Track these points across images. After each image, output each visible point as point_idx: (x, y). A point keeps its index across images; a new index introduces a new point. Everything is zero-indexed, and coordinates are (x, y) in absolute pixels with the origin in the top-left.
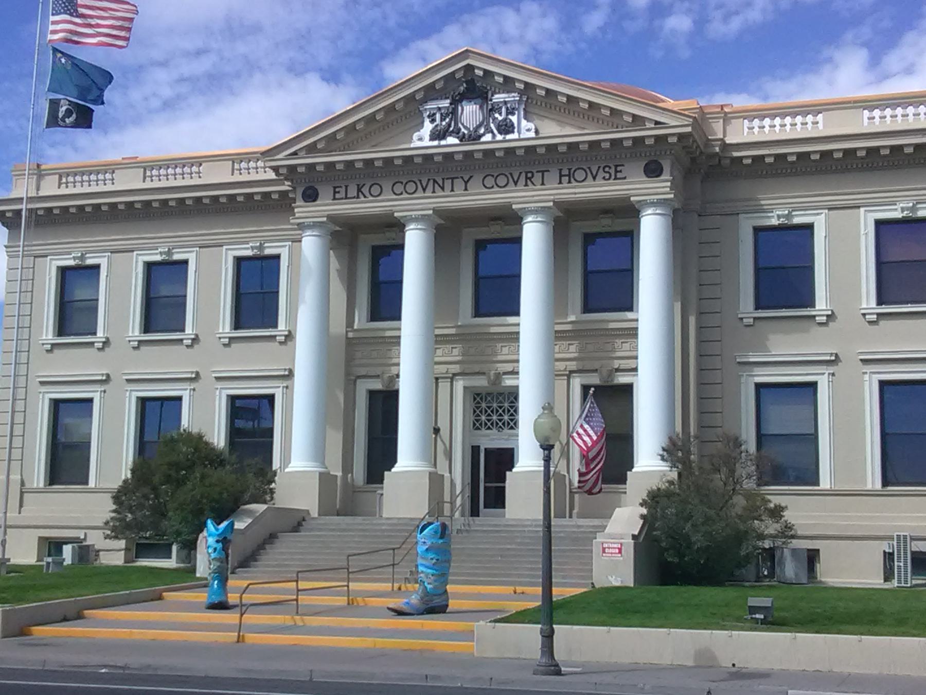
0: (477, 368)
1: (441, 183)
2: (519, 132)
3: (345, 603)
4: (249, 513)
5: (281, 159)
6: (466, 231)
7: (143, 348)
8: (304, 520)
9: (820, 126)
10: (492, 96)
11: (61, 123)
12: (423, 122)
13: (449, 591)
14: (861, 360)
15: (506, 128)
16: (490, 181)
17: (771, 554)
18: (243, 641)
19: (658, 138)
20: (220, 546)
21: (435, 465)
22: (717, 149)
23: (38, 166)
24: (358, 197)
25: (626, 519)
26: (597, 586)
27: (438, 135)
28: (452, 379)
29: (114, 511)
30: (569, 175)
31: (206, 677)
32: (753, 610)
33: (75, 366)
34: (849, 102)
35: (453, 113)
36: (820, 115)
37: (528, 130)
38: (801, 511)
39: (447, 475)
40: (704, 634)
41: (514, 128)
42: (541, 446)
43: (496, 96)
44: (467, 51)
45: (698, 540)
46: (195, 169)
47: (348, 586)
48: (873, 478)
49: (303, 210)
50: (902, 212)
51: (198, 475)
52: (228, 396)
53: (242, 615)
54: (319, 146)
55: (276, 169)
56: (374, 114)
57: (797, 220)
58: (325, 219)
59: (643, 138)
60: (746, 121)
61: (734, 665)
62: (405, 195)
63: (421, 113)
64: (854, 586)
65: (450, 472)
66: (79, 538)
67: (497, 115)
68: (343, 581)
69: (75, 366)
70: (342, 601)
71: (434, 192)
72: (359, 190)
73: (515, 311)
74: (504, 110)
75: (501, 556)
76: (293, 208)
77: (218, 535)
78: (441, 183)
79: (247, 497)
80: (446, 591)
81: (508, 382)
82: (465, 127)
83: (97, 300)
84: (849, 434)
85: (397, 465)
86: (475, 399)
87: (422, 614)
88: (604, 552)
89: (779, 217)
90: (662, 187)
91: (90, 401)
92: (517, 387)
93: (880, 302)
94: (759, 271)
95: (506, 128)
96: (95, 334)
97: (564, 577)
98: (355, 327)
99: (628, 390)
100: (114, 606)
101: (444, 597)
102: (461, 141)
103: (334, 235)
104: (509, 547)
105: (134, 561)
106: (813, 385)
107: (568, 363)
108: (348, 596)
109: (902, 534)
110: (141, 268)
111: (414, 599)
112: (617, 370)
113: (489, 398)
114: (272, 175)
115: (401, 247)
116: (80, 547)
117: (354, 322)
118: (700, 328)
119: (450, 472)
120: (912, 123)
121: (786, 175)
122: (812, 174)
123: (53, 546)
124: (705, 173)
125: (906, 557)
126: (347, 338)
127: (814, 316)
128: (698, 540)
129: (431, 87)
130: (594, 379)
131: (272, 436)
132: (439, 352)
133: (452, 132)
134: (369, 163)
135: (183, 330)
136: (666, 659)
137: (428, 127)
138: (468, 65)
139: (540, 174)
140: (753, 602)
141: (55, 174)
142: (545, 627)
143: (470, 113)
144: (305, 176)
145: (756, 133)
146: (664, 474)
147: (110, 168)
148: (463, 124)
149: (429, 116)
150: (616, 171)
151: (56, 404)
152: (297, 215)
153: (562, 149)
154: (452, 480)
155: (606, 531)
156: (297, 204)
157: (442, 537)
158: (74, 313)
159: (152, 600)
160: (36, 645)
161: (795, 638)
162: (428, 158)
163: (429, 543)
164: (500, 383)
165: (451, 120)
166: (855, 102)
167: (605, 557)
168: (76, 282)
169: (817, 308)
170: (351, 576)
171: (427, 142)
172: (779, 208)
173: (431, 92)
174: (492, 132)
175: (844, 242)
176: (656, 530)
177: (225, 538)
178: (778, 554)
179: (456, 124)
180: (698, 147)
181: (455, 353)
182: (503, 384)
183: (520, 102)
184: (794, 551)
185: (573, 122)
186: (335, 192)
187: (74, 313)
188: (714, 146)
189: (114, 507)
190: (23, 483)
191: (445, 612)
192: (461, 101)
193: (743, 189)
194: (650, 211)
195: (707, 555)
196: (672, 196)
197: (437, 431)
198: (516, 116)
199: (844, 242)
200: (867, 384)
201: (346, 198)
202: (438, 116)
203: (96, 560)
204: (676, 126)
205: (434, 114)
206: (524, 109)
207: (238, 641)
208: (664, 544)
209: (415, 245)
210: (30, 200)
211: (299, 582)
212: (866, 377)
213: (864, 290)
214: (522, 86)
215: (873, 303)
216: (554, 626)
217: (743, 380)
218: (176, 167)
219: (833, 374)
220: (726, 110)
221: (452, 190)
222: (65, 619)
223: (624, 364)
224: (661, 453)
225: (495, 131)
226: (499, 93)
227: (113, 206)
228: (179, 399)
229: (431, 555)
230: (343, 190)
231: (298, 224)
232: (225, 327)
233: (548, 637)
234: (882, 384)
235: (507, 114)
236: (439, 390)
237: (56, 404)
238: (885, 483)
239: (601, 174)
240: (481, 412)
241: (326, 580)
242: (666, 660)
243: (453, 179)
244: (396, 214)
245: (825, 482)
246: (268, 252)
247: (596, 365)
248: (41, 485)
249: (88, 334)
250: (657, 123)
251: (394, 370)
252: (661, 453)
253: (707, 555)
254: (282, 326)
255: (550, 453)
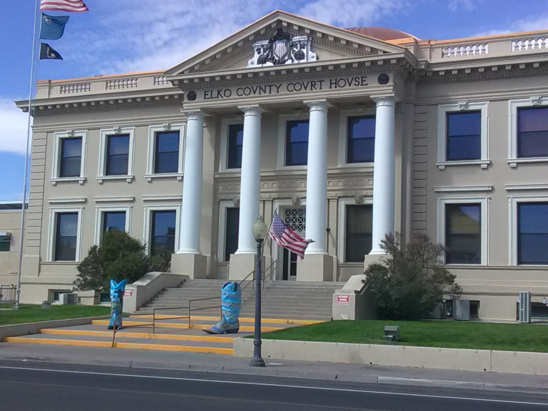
0: (286, 195)
1: (264, 88)
2: (307, 59)
3: (188, 327)
4: (151, 276)
5: (175, 76)
6: (282, 116)
7: (154, 182)
8: (185, 281)
9: (487, 52)
10: (292, 37)
11: (49, 57)
12: (254, 54)
13: (240, 321)
14: (507, 190)
15: (300, 56)
16: (291, 87)
17: (450, 303)
18: (116, 346)
19: (385, 61)
20: (116, 294)
21: (328, 251)
22: (423, 67)
23: (50, 81)
24: (218, 97)
25: (356, 282)
26: (334, 319)
27: (262, 61)
28: (273, 201)
29: (79, 275)
30: (335, 83)
31: (77, 365)
32: (387, 333)
33: (68, 194)
34: (503, 37)
35: (270, 48)
36: (487, 45)
37: (313, 57)
38: (466, 278)
39: (335, 256)
40: (356, 346)
41: (304, 56)
42: (256, 240)
43: (295, 38)
44: (278, 11)
45: (394, 295)
46: (134, 82)
47: (189, 318)
48: (512, 260)
49: (187, 105)
50: (533, 102)
51: (121, 255)
52: (151, 211)
53: (115, 332)
54: (196, 68)
55: (172, 81)
56: (226, 49)
57: (471, 108)
58: (199, 110)
59: (376, 61)
60: (514, 43)
61: (371, 363)
62: (244, 96)
63: (253, 48)
64: (508, 323)
65: (271, 255)
66: (70, 290)
67: (295, 49)
68: (187, 315)
69: (68, 194)
70: (186, 326)
71: (260, 94)
72: (219, 93)
73: (304, 162)
74: (299, 46)
75: (285, 302)
76: (182, 104)
77: (116, 289)
78: (264, 88)
79: (151, 267)
80: (238, 320)
81: (367, 201)
82: (277, 56)
83: (80, 157)
84: (499, 235)
85: (238, 250)
86: (286, 213)
87: (223, 333)
88: (339, 300)
89: (461, 106)
90: (388, 89)
91: (77, 213)
92: (305, 206)
93: (519, 155)
94: (449, 138)
95: (300, 56)
96: (127, 174)
97: (317, 315)
98: (220, 172)
99: (370, 207)
100: (61, 327)
101: (236, 324)
102: (274, 64)
103: (206, 119)
104: (291, 297)
105: (99, 303)
106: (479, 205)
107: (338, 192)
108: (190, 323)
109: (524, 292)
110: (152, 133)
111: (218, 326)
112: (366, 196)
113: (294, 212)
114: (170, 85)
115: (307, 121)
116: (68, 295)
117: (218, 169)
118: (414, 171)
119: (271, 255)
120: (520, 51)
121: (465, 81)
122: (507, 78)
123: (55, 294)
124: (415, 80)
125: (526, 305)
126: (215, 178)
127: (480, 164)
128: (394, 295)
129: (257, 34)
130: (352, 202)
131: (174, 234)
132: (331, 184)
133: (270, 59)
134: (223, 77)
135: (79, 176)
136: (335, 359)
137: (257, 56)
138: (278, 20)
139: (269, 87)
140: (388, 328)
141: (58, 85)
142: (256, 340)
143: (280, 48)
144: (191, 84)
145: (520, 50)
146: (381, 256)
147: (136, 77)
148: (276, 54)
149: (257, 50)
150: (362, 81)
151: (59, 215)
152: (184, 108)
153: (331, 68)
154: (337, 260)
155: (343, 288)
156: (185, 101)
157: (235, 291)
158: (68, 166)
159: (85, 324)
160: (8, 346)
161: (305, 344)
162: (256, 74)
163: (227, 294)
164: (300, 203)
165: (269, 52)
166: (507, 37)
167: (339, 303)
168: (69, 144)
169: (482, 159)
170: (191, 312)
171: (256, 65)
172: (461, 100)
173: (258, 36)
174: (292, 59)
175: (499, 120)
176: (372, 288)
177: (120, 290)
178: (454, 303)
179: (272, 55)
180: (411, 66)
181: (274, 186)
182: (301, 204)
183: (308, 41)
184: (462, 302)
185: (336, 52)
186: (205, 95)
187: (68, 166)
188: (421, 65)
189: (79, 273)
190: (40, 259)
191: (236, 333)
192: (275, 41)
193: (440, 90)
194: (381, 104)
195: (405, 301)
196: (393, 95)
197: (328, 230)
198: (305, 49)
199: (499, 120)
200: (510, 205)
201: (212, 98)
202: (262, 50)
203: (79, 302)
204: (395, 54)
205: (260, 49)
206: (311, 45)
207: (113, 346)
208: (378, 296)
209: (250, 123)
210: (33, 101)
211: (155, 315)
212: (510, 200)
213: (509, 149)
214: (309, 32)
215: (515, 156)
216: (262, 340)
217: (438, 202)
218: (124, 81)
219: (490, 198)
220: (432, 43)
221: (270, 93)
222: (30, 334)
223: (365, 193)
224: (381, 243)
225: (294, 58)
226: (296, 36)
227: (80, 104)
228: (124, 212)
229: (228, 301)
230: (209, 93)
231: (185, 113)
232: (149, 171)
233: (258, 345)
234: (519, 204)
235: (301, 49)
236: (330, 206)
237: (59, 215)
238: (520, 262)
239: (354, 82)
240: (296, 220)
241: (174, 314)
242: (335, 360)
243: (270, 86)
244: (239, 107)
245: (484, 262)
246: (173, 129)
247: (353, 193)
248: (50, 260)
249: (75, 176)
250: (385, 52)
251: (302, 195)
252: (381, 243)
253: (405, 301)
254: (180, 171)
255: (260, 244)
